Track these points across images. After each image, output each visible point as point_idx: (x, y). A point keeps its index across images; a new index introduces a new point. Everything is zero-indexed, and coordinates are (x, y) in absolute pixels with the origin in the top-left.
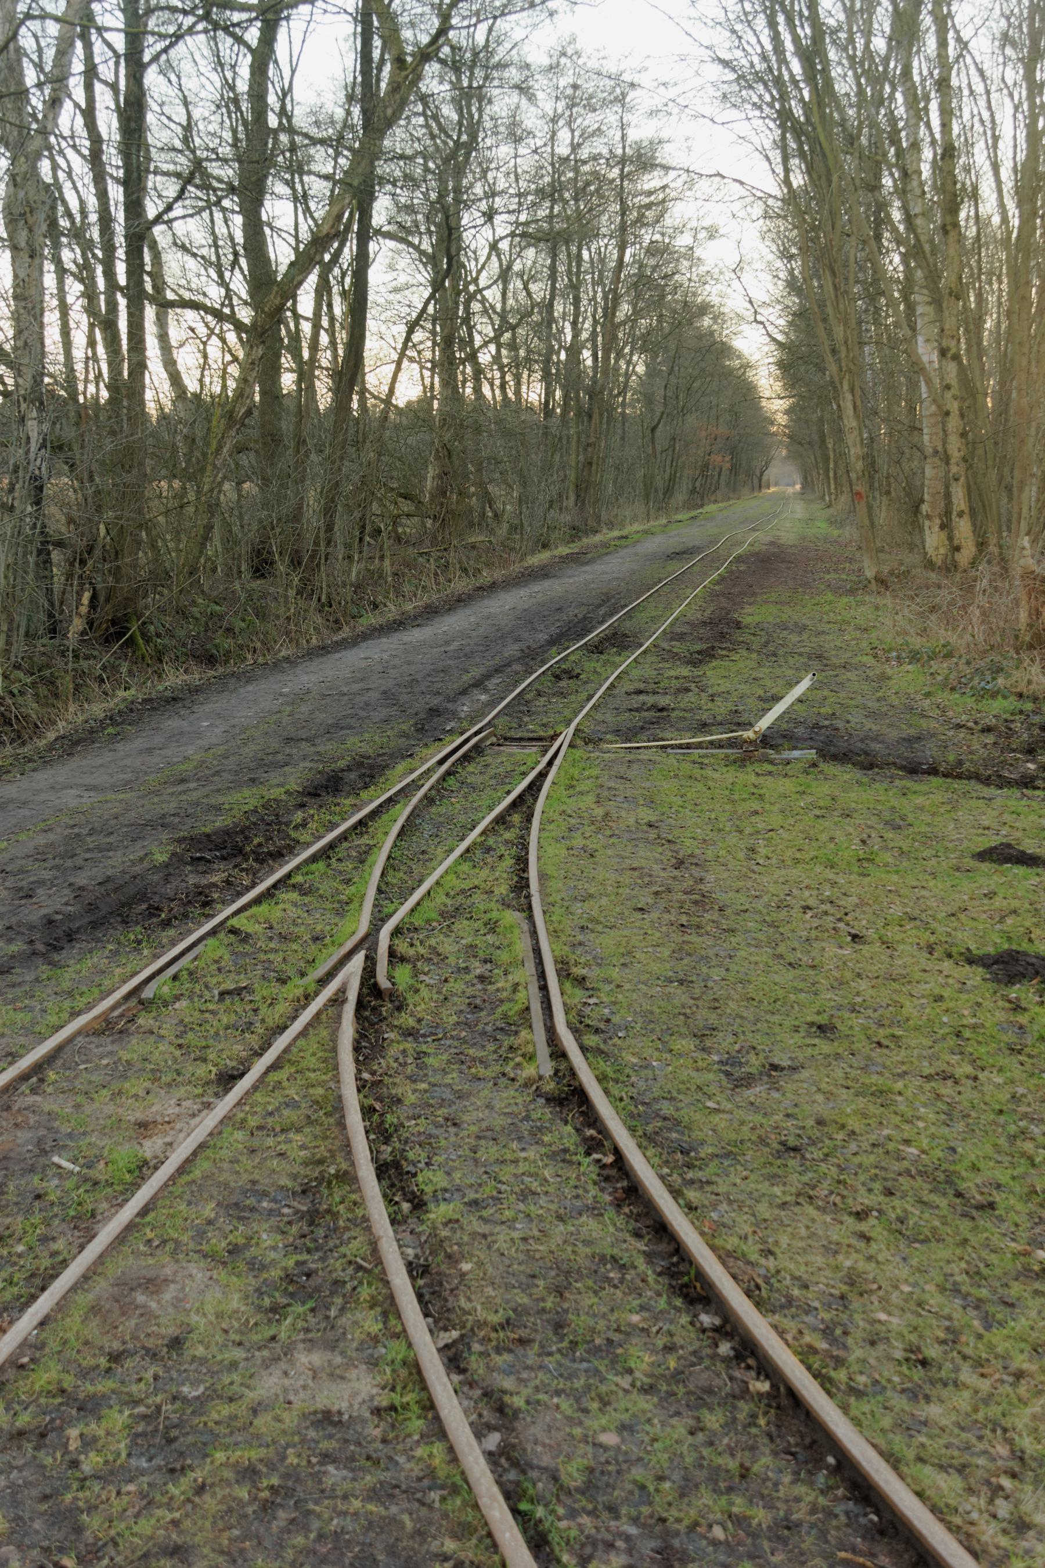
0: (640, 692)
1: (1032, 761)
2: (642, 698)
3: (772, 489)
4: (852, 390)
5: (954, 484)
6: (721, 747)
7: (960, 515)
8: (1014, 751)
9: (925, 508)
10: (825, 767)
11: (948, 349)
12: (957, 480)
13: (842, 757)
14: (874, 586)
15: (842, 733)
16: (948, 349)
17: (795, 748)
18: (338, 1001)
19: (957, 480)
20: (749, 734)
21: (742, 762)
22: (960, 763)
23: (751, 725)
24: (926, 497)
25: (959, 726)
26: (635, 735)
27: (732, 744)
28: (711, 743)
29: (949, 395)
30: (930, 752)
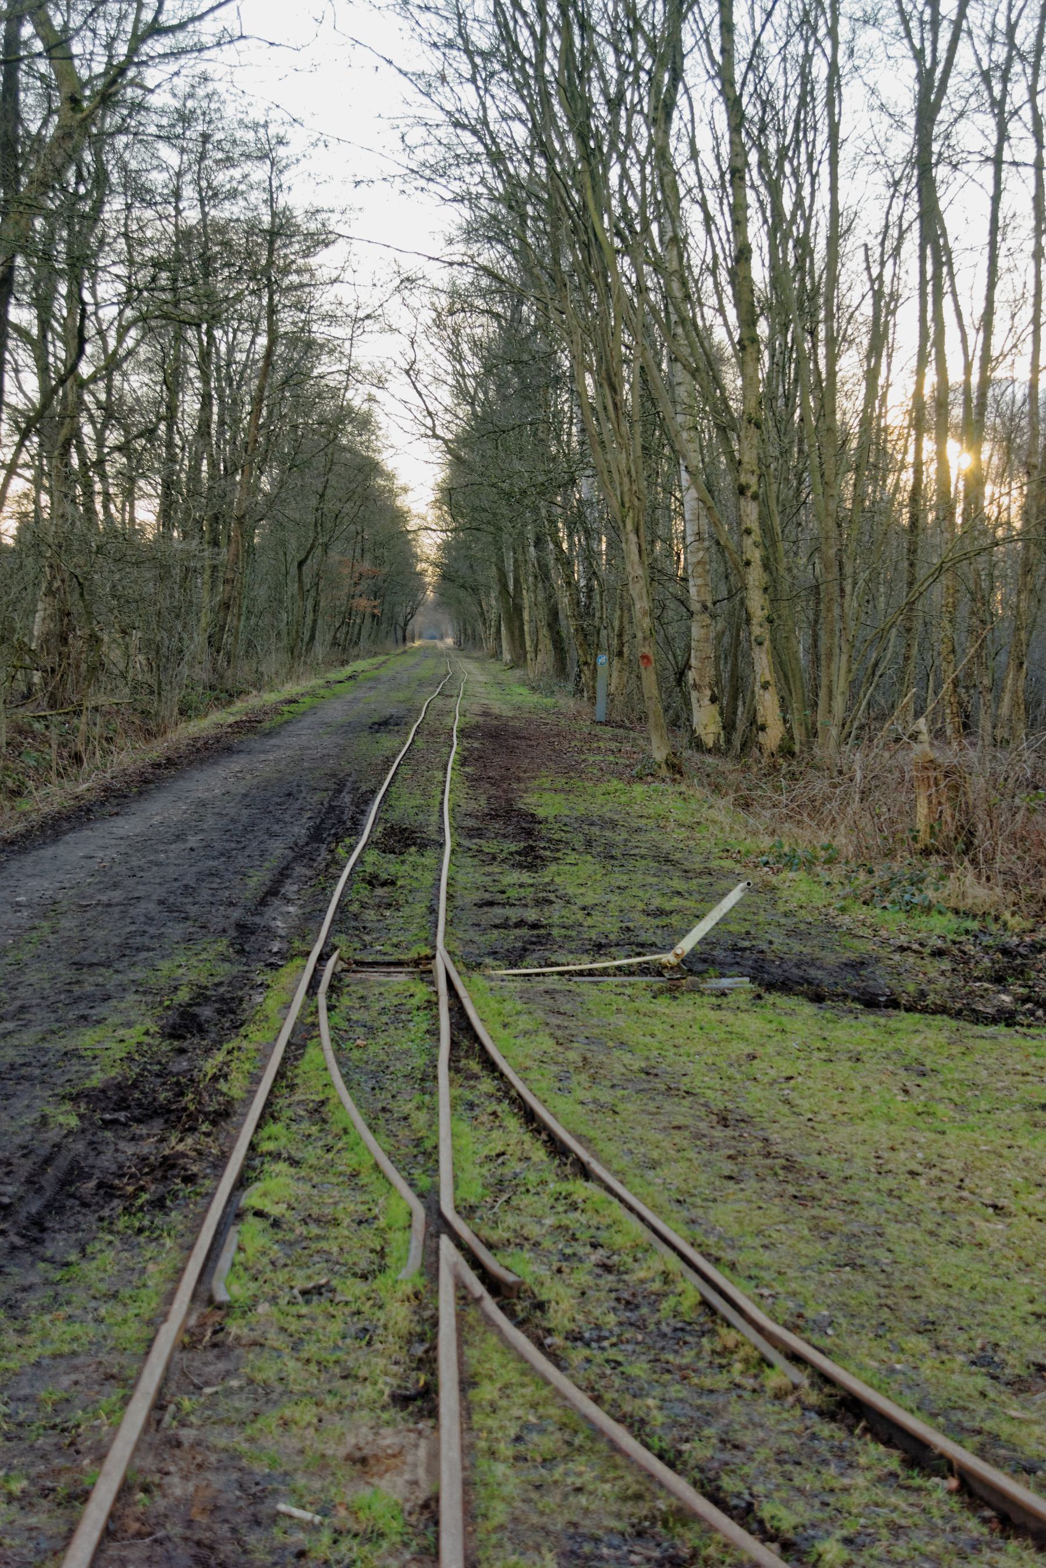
0: (491, 904)
1: (1005, 991)
2: (498, 911)
3: (417, 643)
4: (637, 531)
5: (756, 649)
6: (631, 974)
7: (765, 686)
8: (979, 979)
9: (691, 676)
10: (770, 998)
11: (748, 486)
12: (760, 644)
13: (785, 986)
14: (664, 772)
15: (770, 956)
16: (748, 486)
17: (723, 975)
18: (464, 1299)
19: (760, 644)
20: (668, 958)
21: (672, 991)
22: (923, 994)
23: (672, 946)
24: (693, 662)
25: (902, 949)
26: (522, 957)
27: (644, 970)
28: (619, 968)
29: (748, 541)
30: (882, 982)
